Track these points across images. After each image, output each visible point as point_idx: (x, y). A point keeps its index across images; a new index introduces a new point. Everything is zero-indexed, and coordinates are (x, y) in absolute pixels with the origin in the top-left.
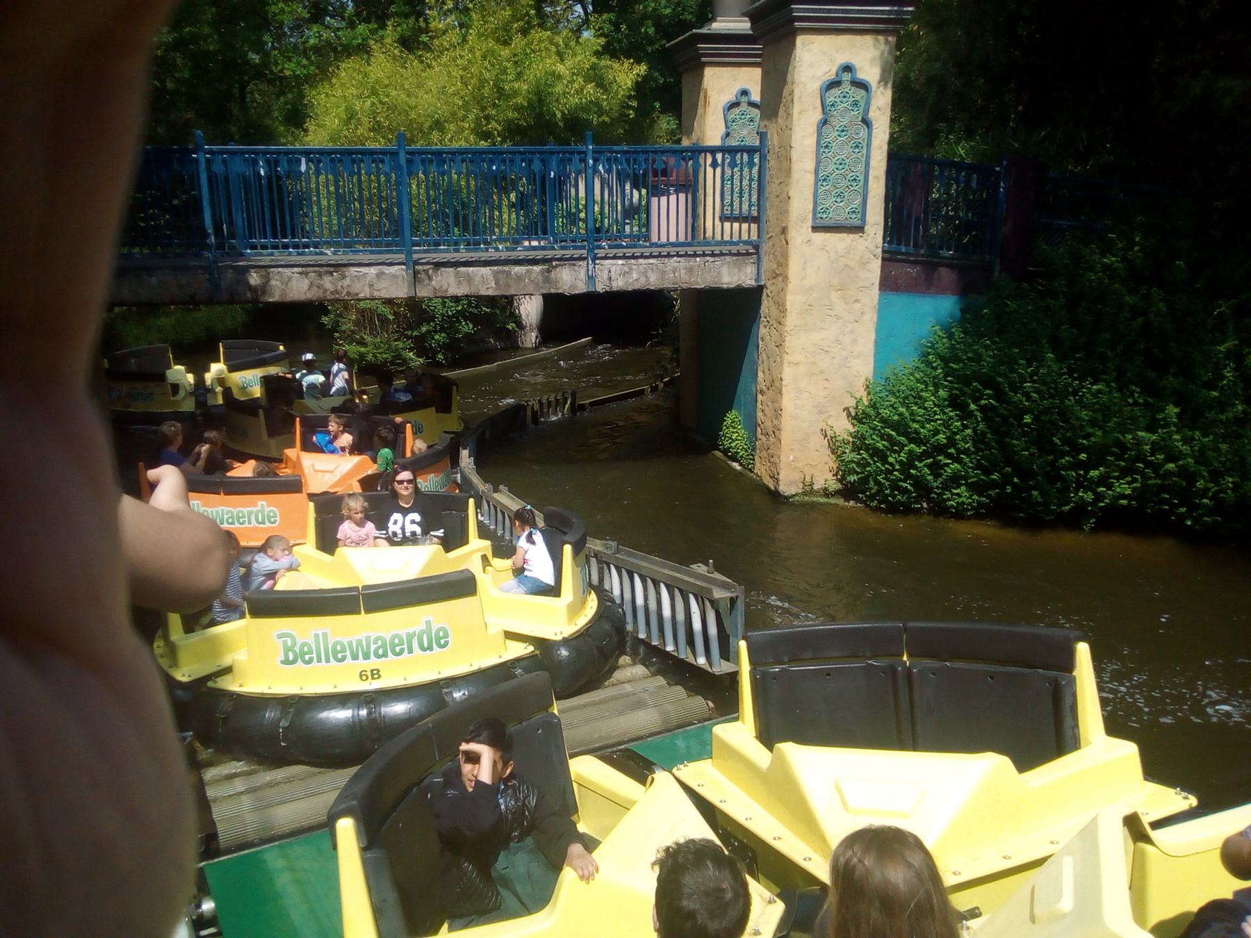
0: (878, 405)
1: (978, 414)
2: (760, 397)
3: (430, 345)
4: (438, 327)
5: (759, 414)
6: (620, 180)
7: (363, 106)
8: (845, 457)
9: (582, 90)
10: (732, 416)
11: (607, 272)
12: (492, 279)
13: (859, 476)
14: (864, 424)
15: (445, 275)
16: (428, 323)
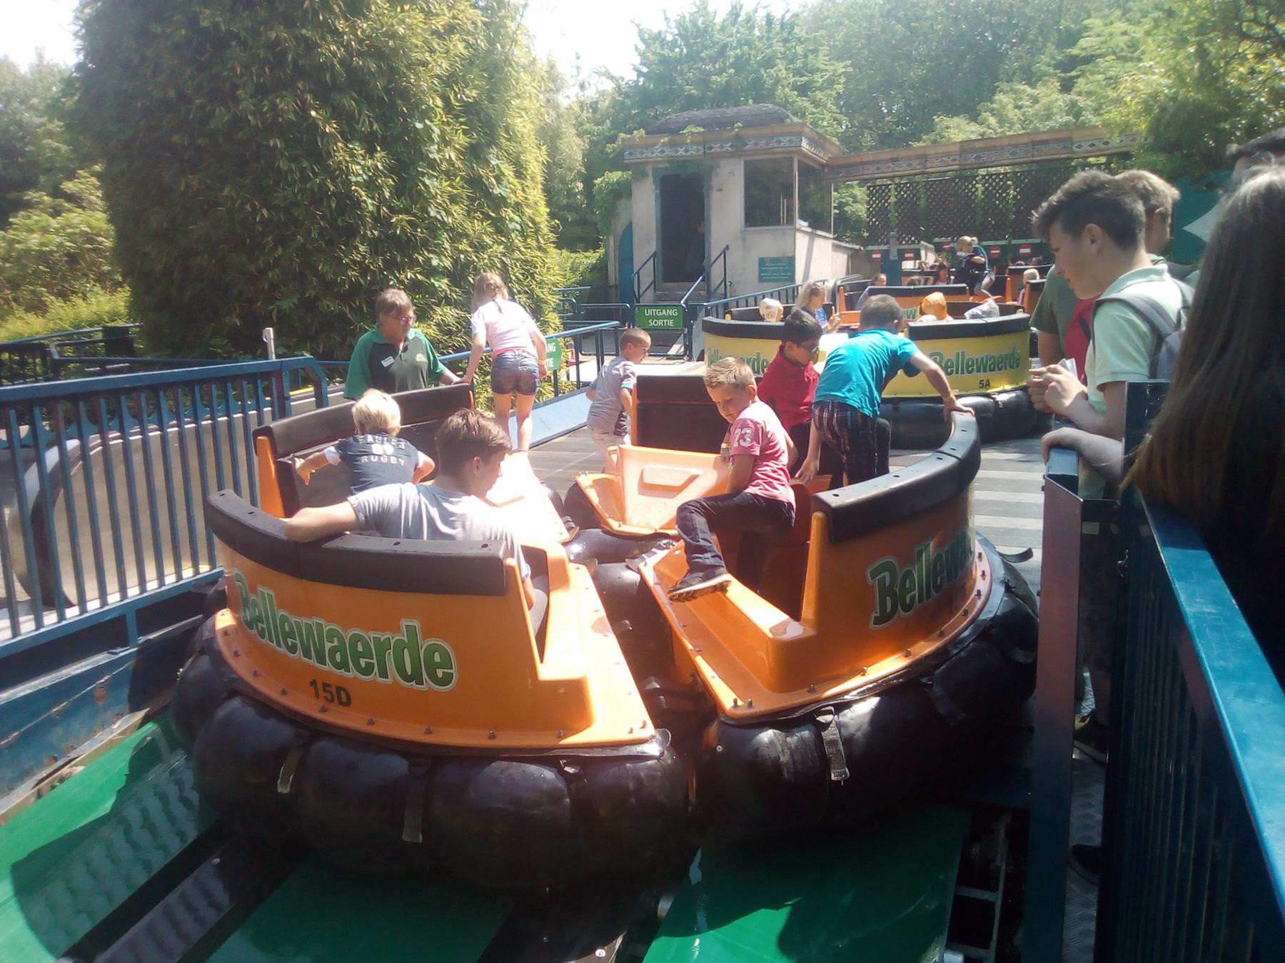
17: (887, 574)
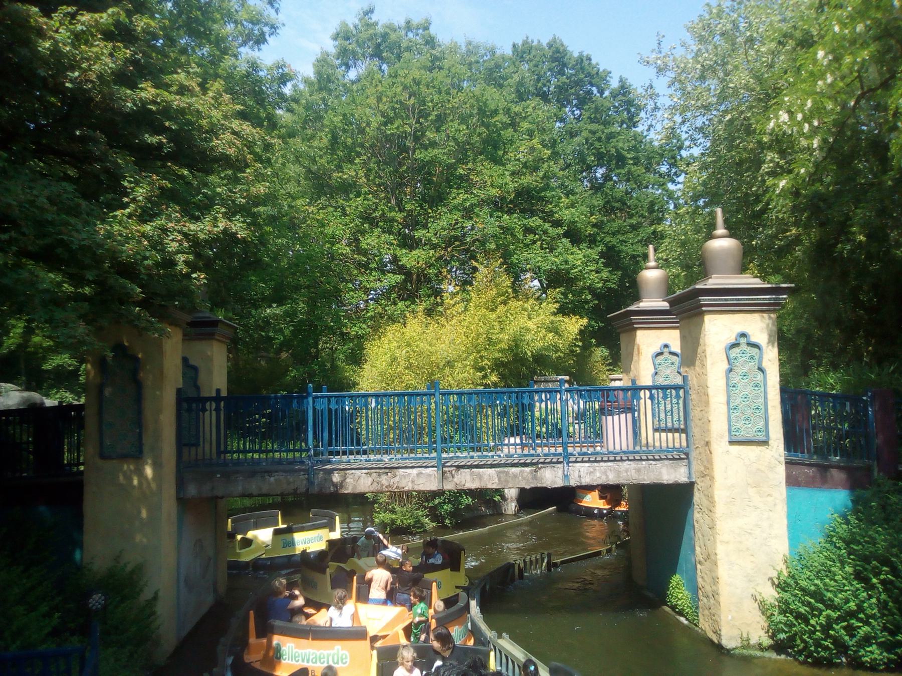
0: (797, 577)
1: (879, 586)
2: (699, 566)
3: (440, 513)
4: (447, 501)
5: (700, 580)
7: (401, 354)
8: (774, 618)
9: (544, 337)
10: (676, 579)
11: (577, 472)
12: (496, 476)
13: (788, 634)
14: (786, 591)
15: (463, 474)
16: (439, 497)
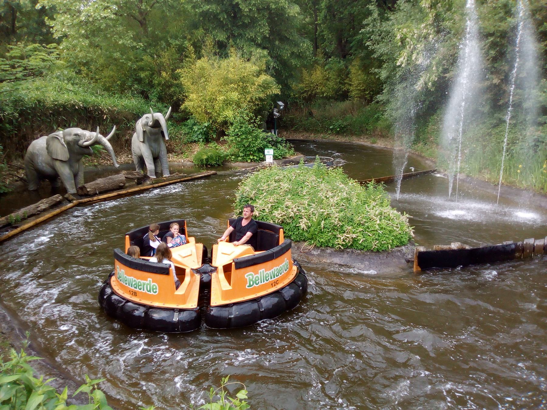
6: (161, 198)
17: (251, 277)
